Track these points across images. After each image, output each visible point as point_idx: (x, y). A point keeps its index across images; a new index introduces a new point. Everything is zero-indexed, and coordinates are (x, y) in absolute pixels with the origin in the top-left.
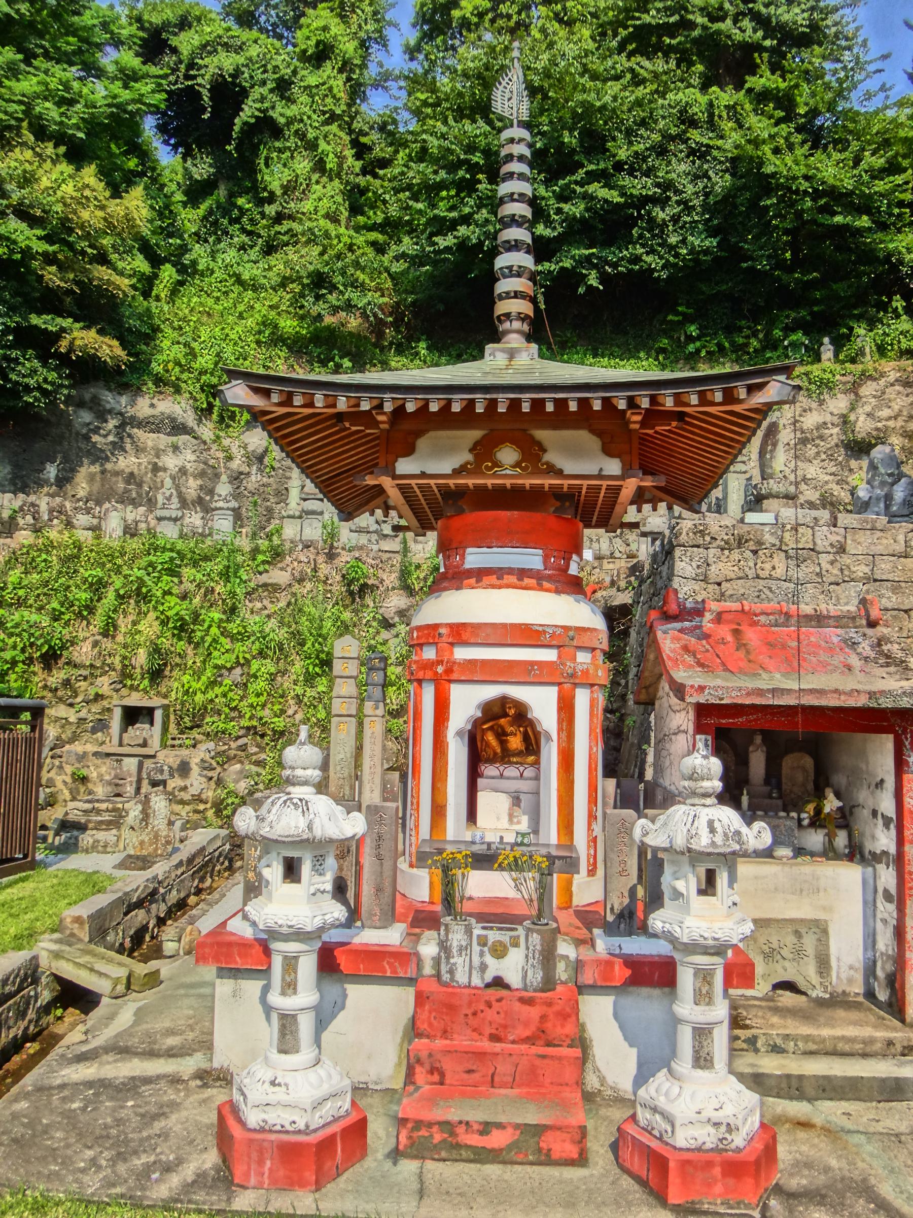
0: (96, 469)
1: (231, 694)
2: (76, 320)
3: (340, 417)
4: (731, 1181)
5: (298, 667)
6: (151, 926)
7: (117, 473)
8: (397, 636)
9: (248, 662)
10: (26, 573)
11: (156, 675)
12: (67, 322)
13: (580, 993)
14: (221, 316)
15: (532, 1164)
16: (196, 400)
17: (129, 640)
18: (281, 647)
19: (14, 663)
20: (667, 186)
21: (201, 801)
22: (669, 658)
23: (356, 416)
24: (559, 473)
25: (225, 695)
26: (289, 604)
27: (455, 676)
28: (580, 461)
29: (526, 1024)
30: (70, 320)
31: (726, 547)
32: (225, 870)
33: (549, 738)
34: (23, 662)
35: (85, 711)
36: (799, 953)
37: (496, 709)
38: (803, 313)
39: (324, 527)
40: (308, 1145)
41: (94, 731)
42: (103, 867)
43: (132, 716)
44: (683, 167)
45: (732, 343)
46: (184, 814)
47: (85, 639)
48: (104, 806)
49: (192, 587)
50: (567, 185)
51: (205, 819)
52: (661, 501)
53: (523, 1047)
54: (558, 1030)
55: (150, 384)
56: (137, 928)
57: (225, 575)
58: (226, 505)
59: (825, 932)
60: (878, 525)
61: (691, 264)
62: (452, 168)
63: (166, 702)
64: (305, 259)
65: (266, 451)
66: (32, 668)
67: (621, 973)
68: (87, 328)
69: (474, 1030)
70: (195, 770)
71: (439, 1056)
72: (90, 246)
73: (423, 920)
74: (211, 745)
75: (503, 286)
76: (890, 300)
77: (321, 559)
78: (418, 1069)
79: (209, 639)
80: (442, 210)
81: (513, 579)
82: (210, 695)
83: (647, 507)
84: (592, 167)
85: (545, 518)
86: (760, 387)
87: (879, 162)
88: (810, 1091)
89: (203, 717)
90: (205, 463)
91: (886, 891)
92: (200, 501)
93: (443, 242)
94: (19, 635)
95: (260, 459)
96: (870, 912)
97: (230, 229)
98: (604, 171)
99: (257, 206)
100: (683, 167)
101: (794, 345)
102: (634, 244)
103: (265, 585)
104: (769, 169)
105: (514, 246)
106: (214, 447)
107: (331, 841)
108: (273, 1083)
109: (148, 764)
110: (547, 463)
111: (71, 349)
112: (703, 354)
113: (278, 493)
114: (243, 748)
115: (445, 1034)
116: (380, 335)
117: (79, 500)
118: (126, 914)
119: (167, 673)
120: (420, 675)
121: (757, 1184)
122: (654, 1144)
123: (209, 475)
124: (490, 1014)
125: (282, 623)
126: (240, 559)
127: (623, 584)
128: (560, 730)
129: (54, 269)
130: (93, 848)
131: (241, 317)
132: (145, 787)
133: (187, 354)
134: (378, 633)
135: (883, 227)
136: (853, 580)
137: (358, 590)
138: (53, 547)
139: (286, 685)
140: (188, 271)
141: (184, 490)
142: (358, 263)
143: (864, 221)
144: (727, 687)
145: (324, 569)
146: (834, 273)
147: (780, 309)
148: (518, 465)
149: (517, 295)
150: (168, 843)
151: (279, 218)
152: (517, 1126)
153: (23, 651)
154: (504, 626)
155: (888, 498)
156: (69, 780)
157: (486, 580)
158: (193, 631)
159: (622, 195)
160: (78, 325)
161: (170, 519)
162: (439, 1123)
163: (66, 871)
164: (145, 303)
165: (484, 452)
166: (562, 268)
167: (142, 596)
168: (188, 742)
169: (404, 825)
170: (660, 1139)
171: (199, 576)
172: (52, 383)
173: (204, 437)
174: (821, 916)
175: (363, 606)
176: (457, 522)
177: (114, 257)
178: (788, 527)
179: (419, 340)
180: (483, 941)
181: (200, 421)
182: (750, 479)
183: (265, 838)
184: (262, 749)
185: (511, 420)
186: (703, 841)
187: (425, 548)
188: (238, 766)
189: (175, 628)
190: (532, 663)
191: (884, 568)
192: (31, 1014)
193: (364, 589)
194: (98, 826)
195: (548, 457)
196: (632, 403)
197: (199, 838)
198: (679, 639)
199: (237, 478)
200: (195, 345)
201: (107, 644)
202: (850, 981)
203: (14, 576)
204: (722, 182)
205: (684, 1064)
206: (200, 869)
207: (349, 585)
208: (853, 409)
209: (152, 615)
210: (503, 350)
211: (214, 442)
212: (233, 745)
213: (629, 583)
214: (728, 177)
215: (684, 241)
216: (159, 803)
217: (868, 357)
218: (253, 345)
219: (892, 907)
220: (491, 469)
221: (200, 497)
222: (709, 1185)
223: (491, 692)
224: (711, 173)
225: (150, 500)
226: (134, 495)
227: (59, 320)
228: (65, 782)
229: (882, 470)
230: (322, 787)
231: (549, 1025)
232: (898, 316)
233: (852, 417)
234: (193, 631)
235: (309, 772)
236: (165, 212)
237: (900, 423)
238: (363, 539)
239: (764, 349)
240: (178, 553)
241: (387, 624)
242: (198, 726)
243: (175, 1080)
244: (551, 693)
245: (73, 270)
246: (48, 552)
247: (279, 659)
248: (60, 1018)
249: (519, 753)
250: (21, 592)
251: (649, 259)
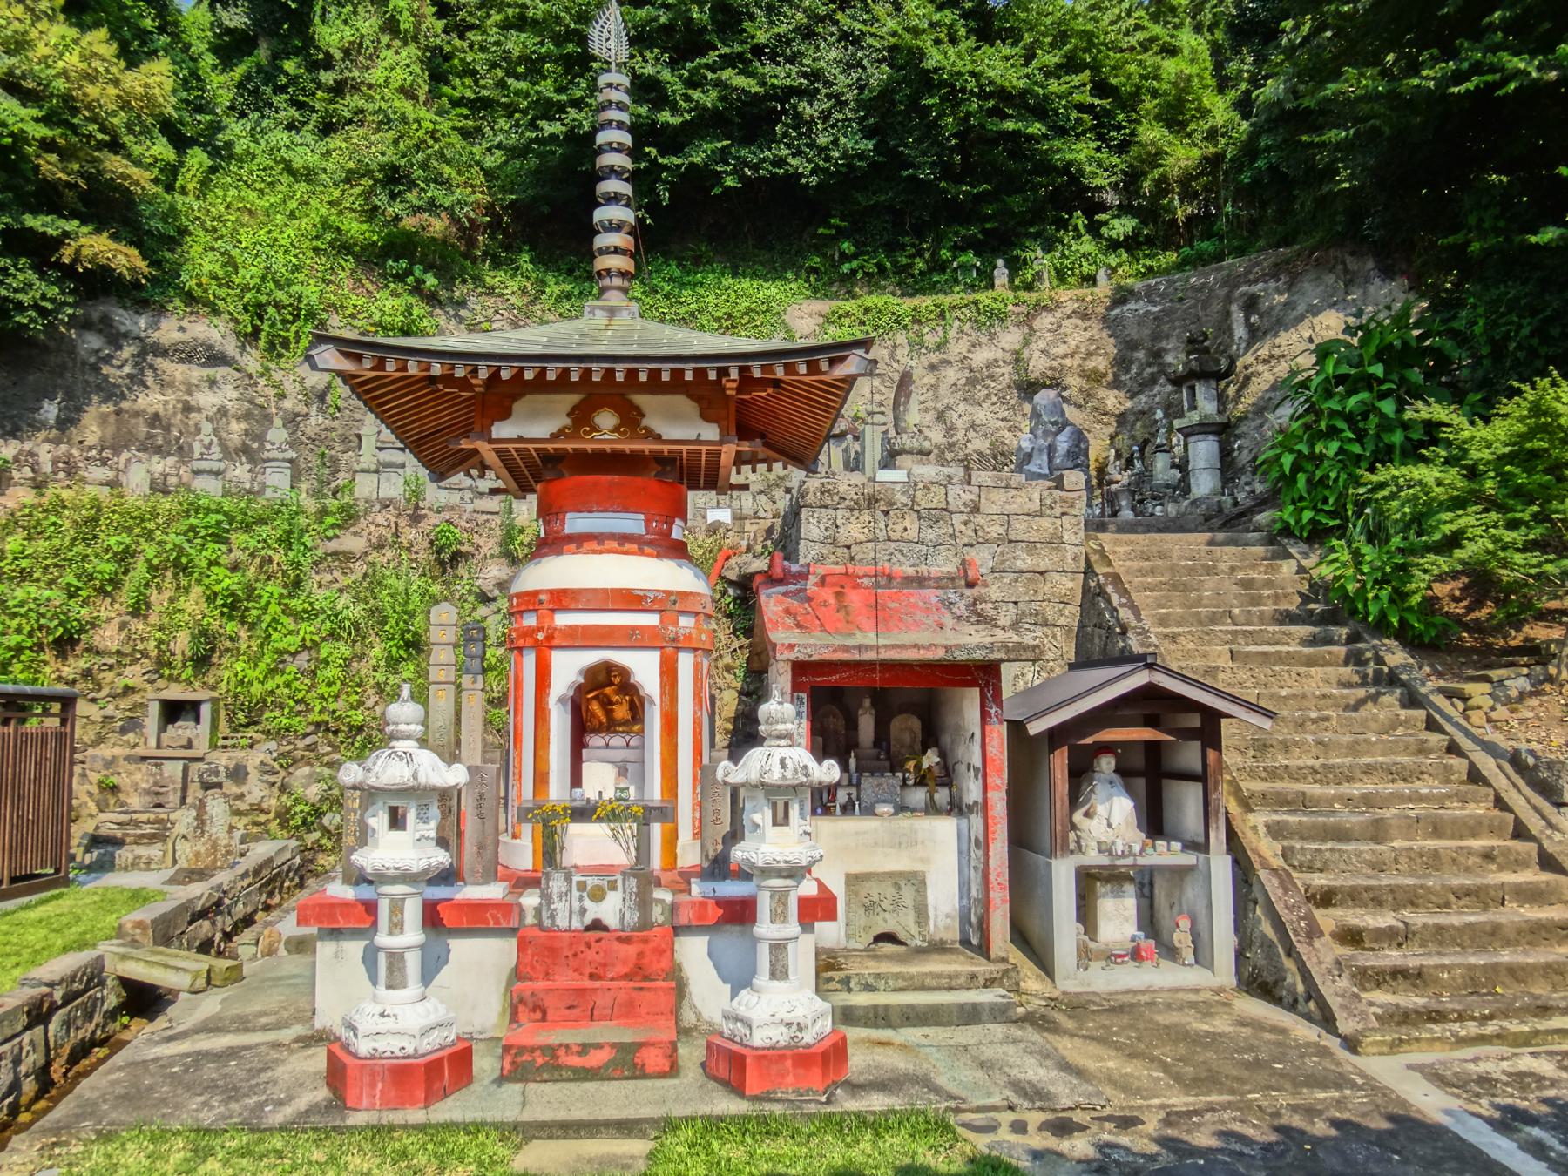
0: (108, 408)
1: (296, 684)
2: (84, 223)
3: (432, 380)
4: (801, 1071)
5: (377, 651)
6: (217, 939)
7: (137, 414)
8: (499, 611)
9: (316, 644)
10: (29, 539)
11: (201, 662)
12: (71, 225)
13: (676, 935)
14: (264, 213)
15: (628, 1078)
16: (237, 322)
17: (166, 621)
18: (356, 625)
19: (19, 649)
20: (815, 76)
21: (262, 811)
22: (771, 621)
23: (448, 379)
24: (658, 438)
25: (288, 685)
26: (365, 575)
27: (556, 642)
28: (679, 426)
29: (624, 962)
30: (76, 223)
31: (856, 507)
32: (296, 887)
33: (652, 702)
34: (31, 649)
35: (111, 707)
36: (898, 904)
37: (601, 678)
38: (973, 230)
39: (407, 483)
40: (418, 1065)
41: (123, 731)
42: (148, 881)
43: (174, 711)
44: (833, 54)
45: (894, 263)
46: (240, 826)
47: (109, 620)
48: (144, 817)
49: (244, 556)
50: (697, 69)
51: (268, 832)
52: (776, 460)
53: (622, 983)
54: (656, 965)
55: (178, 302)
56: (211, 927)
57: (286, 541)
58: (281, 456)
59: (924, 883)
60: (1012, 483)
61: (844, 170)
62: (559, 40)
63: (215, 694)
64: (379, 149)
65: (329, 387)
66: (42, 657)
67: (715, 913)
68: (98, 231)
69: (576, 970)
70: (254, 775)
71: (541, 995)
72: (100, 130)
73: (524, 882)
74: (273, 745)
75: (601, 241)
76: (1071, 216)
77: (403, 523)
78: (521, 1008)
79: (267, 618)
80: (546, 88)
81: (614, 545)
82: (270, 685)
83: (746, 469)
84: (725, 50)
85: (647, 482)
86: (842, 359)
87: (1053, 59)
88: (894, 1019)
89: (262, 710)
90: (251, 402)
91: (977, 839)
92: (245, 450)
93: (550, 128)
94: (25, 616)
95: (321, 397)
96: (965, 862)
97: (275, 99)
98: (740, 56)
99: (309, 71)
100: (833, 54)
101: (964, 267)
102: (780, 142)
103: (335, 554)
104: (929, 64)
105: (614, 199)
106: (262, 382)
107: (434, 789)
108: (382, 1015)
109: (195, 767)
110: (646, 428)
111: (77, 259)
112: (859, 276)
113: (344, 439)
114: (312, 748)
115: (547, 976)
116: (472, 243)
117: (91, 448)
118: (190, 923)
119: (214, 660)
120: (521, 643)
121: (825, 1075)
122: (734, 1047)
123: (257, 416)
124: (590, 955)
125: (357, 599)
126: (302, 521)
127: (759, 548)
128: (663, 694)
129: (53, 158)
130: (134, 865)
131: (292, 216)
132: (195, 791)
133: (225, 265)
134: (474, 609)
135: (1062, 132)
136: (987, 541)
137: (448, 559)
138: (64, 507)
139: (363, 672)
140: (222, 155)
141: (224, 435)
142: (443, 155)
143: (1037, 128)
144: (818, 645)
145: (409, 534)
146: (1010, 184)
147: (948, 224)
148: (616, 430)
149: (616, 251)
150: (229, 853)
151: (339, 89)
152: (613, 1046)
153: (30, 635)
154: (605, 591)
155: (1051, 449)
156: (95, 790)
157: (586, 546)
158: (247, 609)
159: (763, 83)
160: (85, 229)
161: (210, 472)
162: (541, 1048)
163: (107, 889)
164: (168, 197)
165: (581, 417)
166: (692, 164)
167: (182, 568)
168: (244, 742)
169: (506, 805)
170: (741, 1044)
171: (253, 543)
172: (53, 300)
173: (250, 370)
174: (918, 867)
175: (456, 577)
176: (557, 486)
177: (127, 139)
178: (920, 485)
179: (521, 251)
180: (582, 886)
181: (243, 348)
182: (886, 432)
183: (372, 787)
184: (336, 748)
185: (607, 386)
186: (775, 776)
187: (526, 510)
188: (307, 769)
189: (223, 606)
190: (634, 628)
191: (1020, 528)
192: (98, 1018)
193: (457, 557)
194: (140, 838)
195: (645, 422)
196: (723, 372)
197: (262, 850)
198: (781, 602)
199: (293, 420)
200: (235, 253)
201: (138, 626)
202: (947, 928)
203: (13, 543)
204: (879, 75)
205: (762, 979)
206: (268, 882)
207: (438, 553)
208: (1026, 344)
209: (197, 591)
210: (602, 308)
211: (262, 375)
212: (300, 744)
213: (765, 547)
214: (884, 67)
215: (835, 142)
216: (217, 807)
217: (1047, 284)
218: (311, 254)
219: (980, 853)
220: (588, 433)
221: (244, 444)
222: (783, 1076)
223: (592, 657)
224: (865, 62)
225: (181, 448)
226: (160, 441)
227: (62, 223)
228: (90, 794)
229: (1045, 418)
230: (423, 742)
231: (645, 961)
232: (1078, 236)
233: (1026, 354)
234: (247, 609)
235: (412, 727)
236: (191, 80)
237: (1077, 361)
238: (455, 498)
239: (931, 270)
240: (226, 514)
241: (485, 599)
242: (255, 723)
243: (277, 1046)
244: (655, 656)
245: (78, 159)
246: (57, 514)
247: (354, 641)
248: (126, 1027)
249: (625, 723)
250: (24, 563)
251: (794, 162)
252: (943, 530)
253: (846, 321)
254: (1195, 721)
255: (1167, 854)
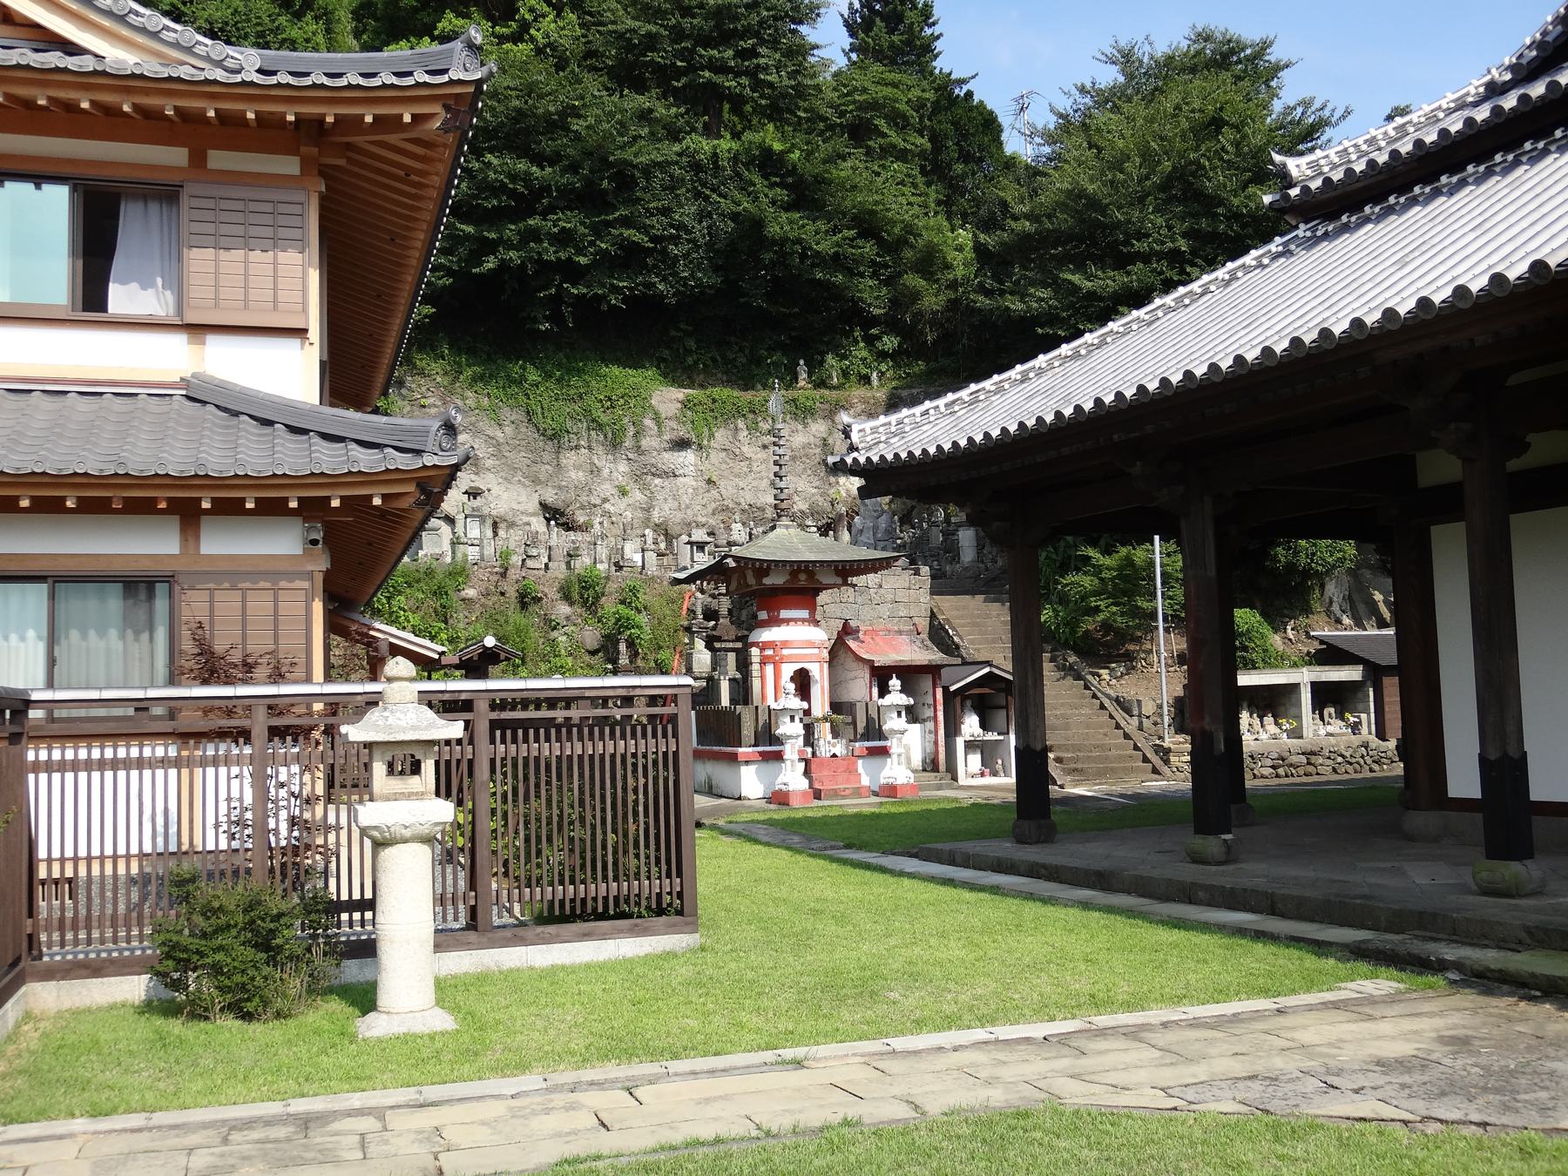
20: (681, 226)
81: (117, 496)
223: (798, 666)
233: (830, 441)
252: (866, 597)
253: (700, 408)
254: (1003, 685)
255: (992, 736)
